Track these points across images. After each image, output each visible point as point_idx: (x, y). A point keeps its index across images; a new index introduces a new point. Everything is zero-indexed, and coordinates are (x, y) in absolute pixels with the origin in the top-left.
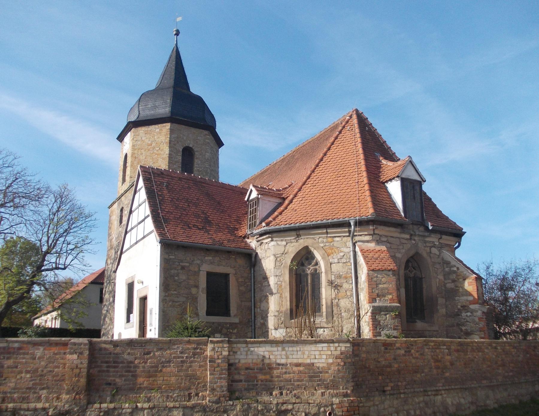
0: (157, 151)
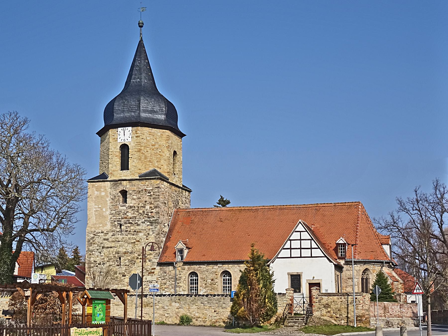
0: (160, 152)
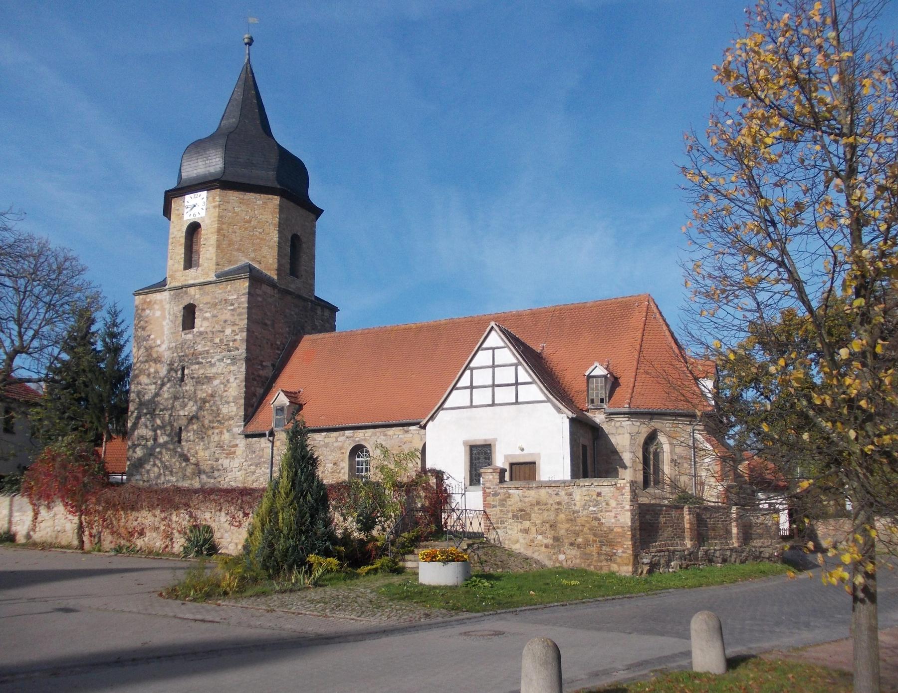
0: (260, 233)
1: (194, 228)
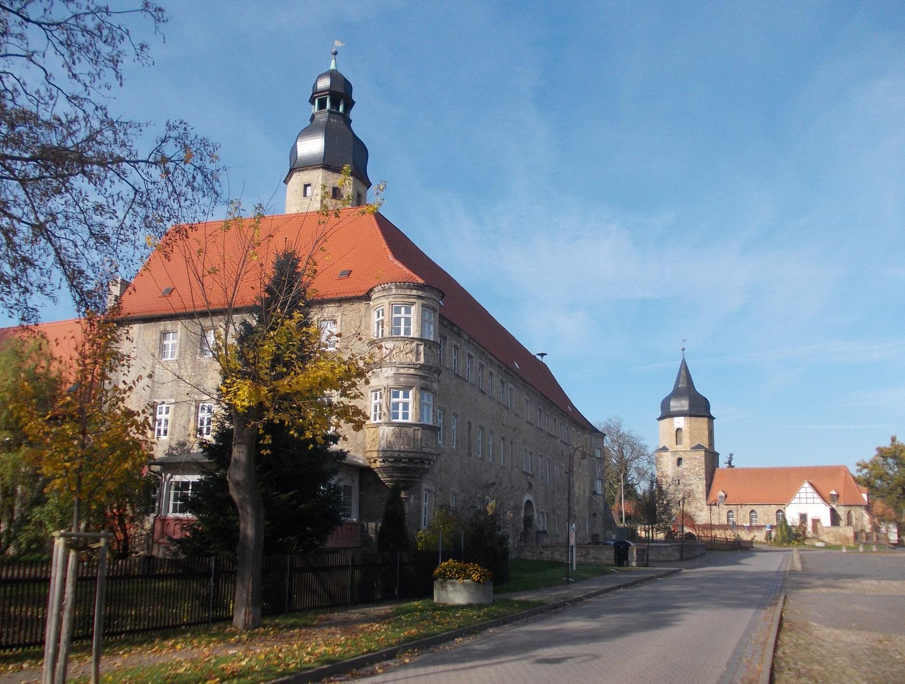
1: (679, 430)
